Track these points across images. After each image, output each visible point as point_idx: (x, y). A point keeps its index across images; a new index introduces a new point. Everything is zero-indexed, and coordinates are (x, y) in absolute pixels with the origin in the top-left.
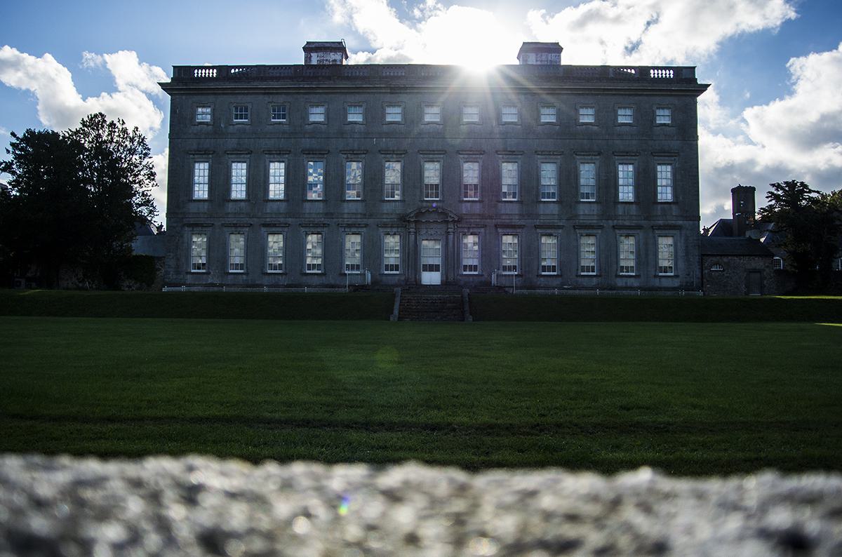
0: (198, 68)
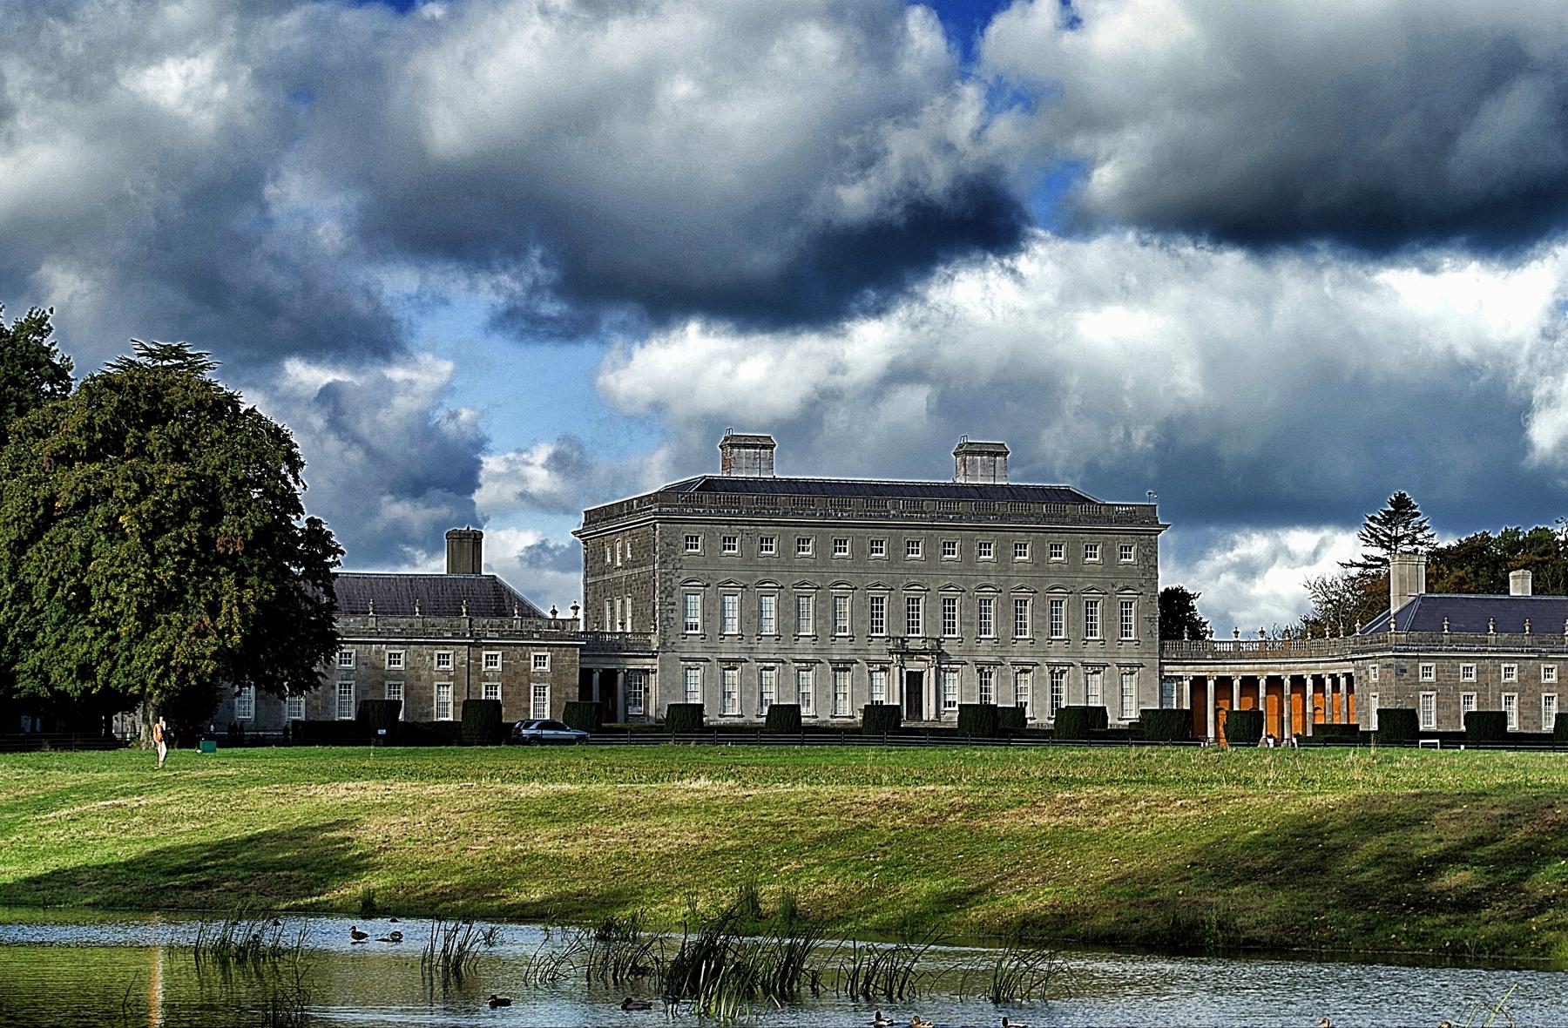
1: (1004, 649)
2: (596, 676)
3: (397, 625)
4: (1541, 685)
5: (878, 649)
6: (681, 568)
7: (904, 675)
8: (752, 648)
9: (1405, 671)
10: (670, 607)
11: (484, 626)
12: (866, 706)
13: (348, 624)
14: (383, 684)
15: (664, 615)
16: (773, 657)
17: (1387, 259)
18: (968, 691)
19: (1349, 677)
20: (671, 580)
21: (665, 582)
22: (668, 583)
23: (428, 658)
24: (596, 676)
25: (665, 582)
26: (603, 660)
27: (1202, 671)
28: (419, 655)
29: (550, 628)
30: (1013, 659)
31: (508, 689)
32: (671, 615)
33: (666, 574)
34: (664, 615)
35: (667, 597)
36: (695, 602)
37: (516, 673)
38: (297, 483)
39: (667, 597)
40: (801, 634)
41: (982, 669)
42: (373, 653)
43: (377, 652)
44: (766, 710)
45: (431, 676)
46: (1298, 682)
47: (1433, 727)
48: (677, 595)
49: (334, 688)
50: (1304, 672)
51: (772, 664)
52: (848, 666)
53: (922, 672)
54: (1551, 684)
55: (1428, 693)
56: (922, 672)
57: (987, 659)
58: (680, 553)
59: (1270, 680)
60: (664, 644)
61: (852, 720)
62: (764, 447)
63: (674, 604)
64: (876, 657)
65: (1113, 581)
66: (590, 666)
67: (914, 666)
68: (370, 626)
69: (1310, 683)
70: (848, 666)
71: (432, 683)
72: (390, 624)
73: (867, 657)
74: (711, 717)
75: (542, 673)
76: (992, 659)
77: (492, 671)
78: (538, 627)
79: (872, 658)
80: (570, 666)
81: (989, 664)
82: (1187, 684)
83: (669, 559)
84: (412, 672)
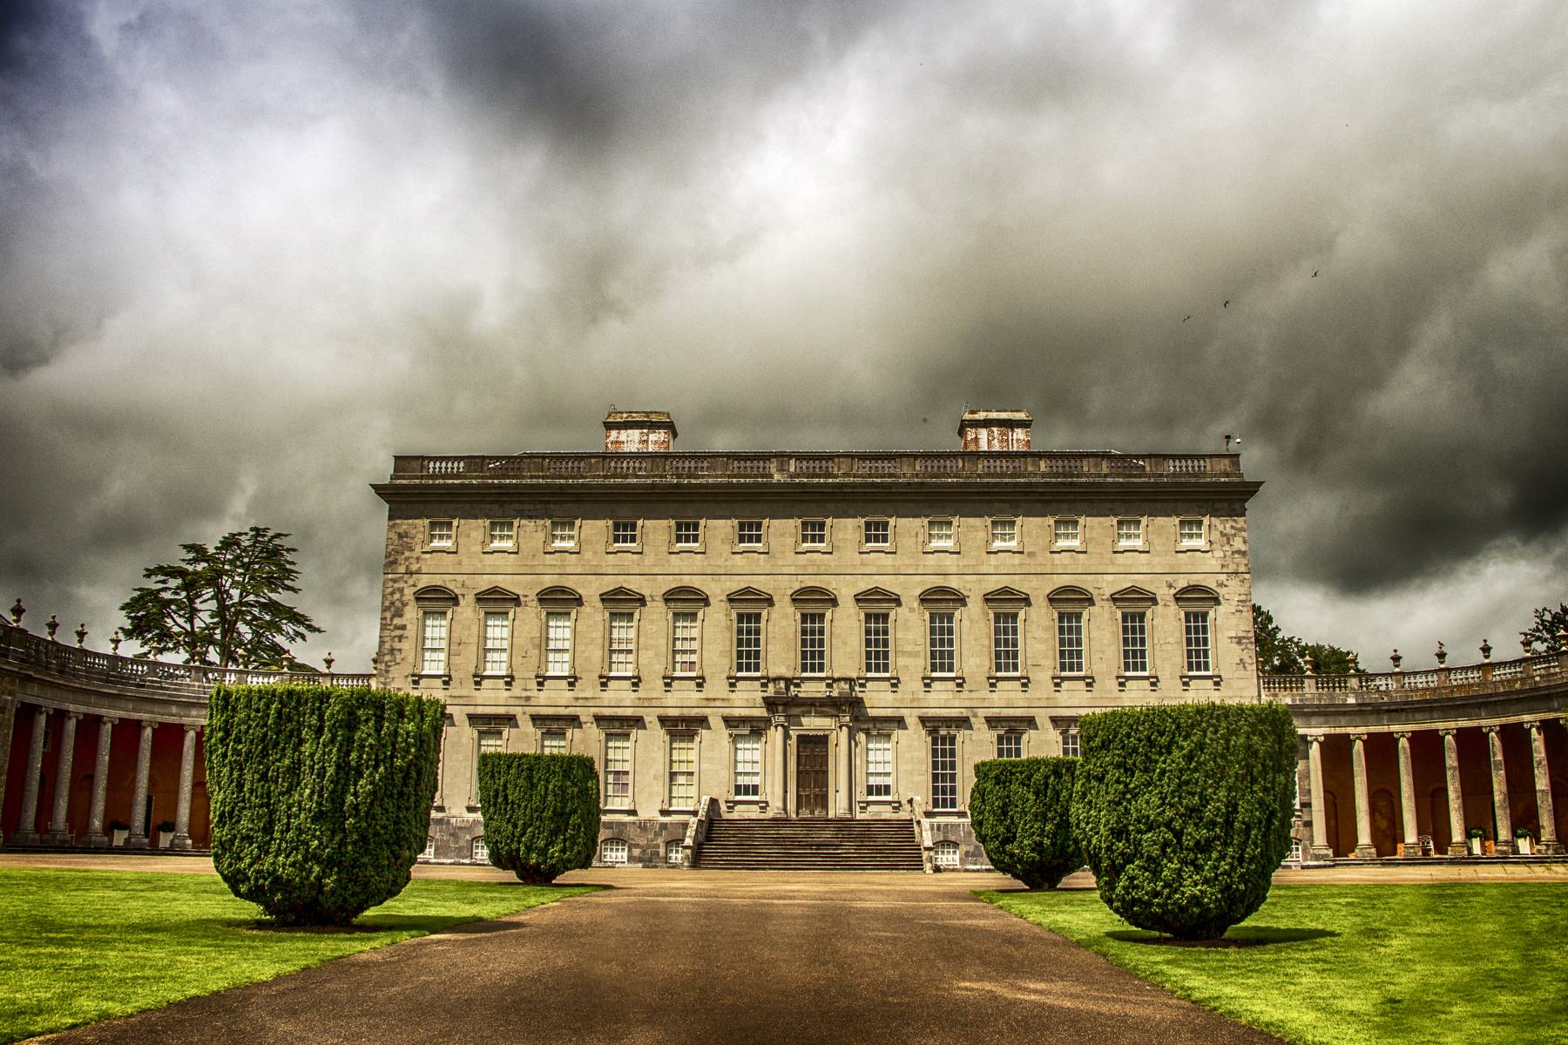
0: (435, 459)
1: (974, 695)
2: (71, 725)
7: (793, 742)
8: (528, 698)
10: (398, 632)
15: (387, 646)
17: (1535, 546)
18: (909, 767)
20: (401, 590)
21: (392, 593)
22: (397, 596)
24: (71, 725)
25: (392, 593)
32: (397, 645)
33: (395, 581)
34: (387, 646)
35: (393, 617)
38: (256, 601)
39: (393, 617)
40: (612, 674)
58: (418, 549)
61: (632, 818)
66: (135, 716)
67: (813, 723)
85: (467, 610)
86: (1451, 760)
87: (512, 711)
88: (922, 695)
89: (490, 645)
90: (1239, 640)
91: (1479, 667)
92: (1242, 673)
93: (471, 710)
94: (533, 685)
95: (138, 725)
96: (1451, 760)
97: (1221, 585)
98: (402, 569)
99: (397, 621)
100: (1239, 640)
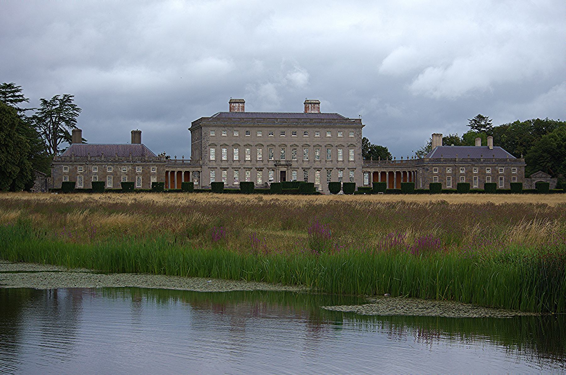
2: (169, 173)
3: (110, 159)
4: (473, 174)
5: (271, 165)
6: (209, 140)
8: (231, 164)
9: (428, 170)
11: (137, 159)
12: (223, 183)
13: (95, 159)
14: (106, 176)
16: (238, 167)
19: (416, 171)
20: (206, 144)
23: (119, 169)
24: (169, 173)
26: (185, 168)
27: (377, 170)
28: (117, 168)
29: (156, 159)
30: (314, 167)
31: (144, 178)
36: (213, 151)
37: (146, 173)
41: (305, 170)
42: (103, 167)
43: (104, 167)
44: (548, 182)
45: (121, 174)
46: (405, 173)
47: (82, 187)
48: (208, 148)
49: (91, 178)
50: (406, 170)
51: (238, 169)
52: (262, 169)
53: (285, 171)
54: (476, 174)
55: (436, 177)
56: (285, 171)
57: (307, 167)
59: (389, 173)
60: (204, 163)
62: (241, 103)
63: (207, 151)
64: (271, 167)
65: (347, 143)
68: (102, 159)
69: (402, 173)
70: (262, 169)
71: (121, 176)
72: (108, 159)
73: (268, 167)
74: (226, 187)
75: (154, 173)
76: (308, 167)
77: (139, 172)
78: (153, 159)
79: (269, 167)
80: (163, 171)
81: (307, 168)
82: (372, 174)
83: (205, 138)
84: (115, 173)
85: (312, 147)
86: (395, 176)
87: (217, 167)
88: (302, 164)
89: (342, 157)
90: (359, 154)
91: (400, 161)
92: (359, 160)
93: (221, 167)
94: (232, 162)
95: (181, 172)
96: (395, 176)
97: (356, 144)
98: (206, 140)
99: (206, 150)
100: (359, 154)
